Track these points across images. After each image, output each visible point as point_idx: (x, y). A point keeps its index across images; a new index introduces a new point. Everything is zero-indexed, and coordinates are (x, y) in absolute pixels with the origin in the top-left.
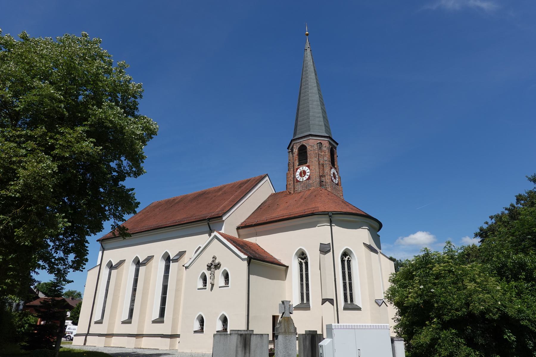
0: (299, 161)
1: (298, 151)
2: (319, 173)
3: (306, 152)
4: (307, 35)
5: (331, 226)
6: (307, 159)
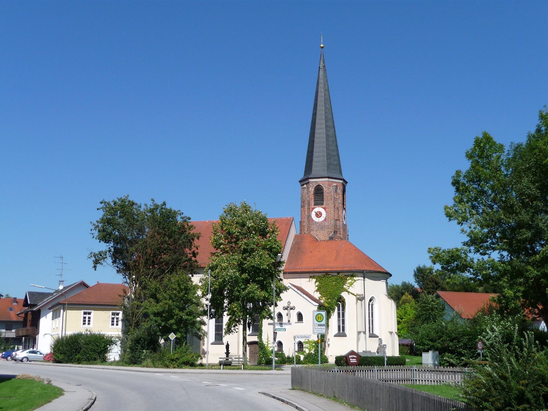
0: (315, 201)
1: (314, 189)
2: (334, 216)
3: (322, 193)
4: (322, 48)
5: (364, 278)
6: (323, 200)
